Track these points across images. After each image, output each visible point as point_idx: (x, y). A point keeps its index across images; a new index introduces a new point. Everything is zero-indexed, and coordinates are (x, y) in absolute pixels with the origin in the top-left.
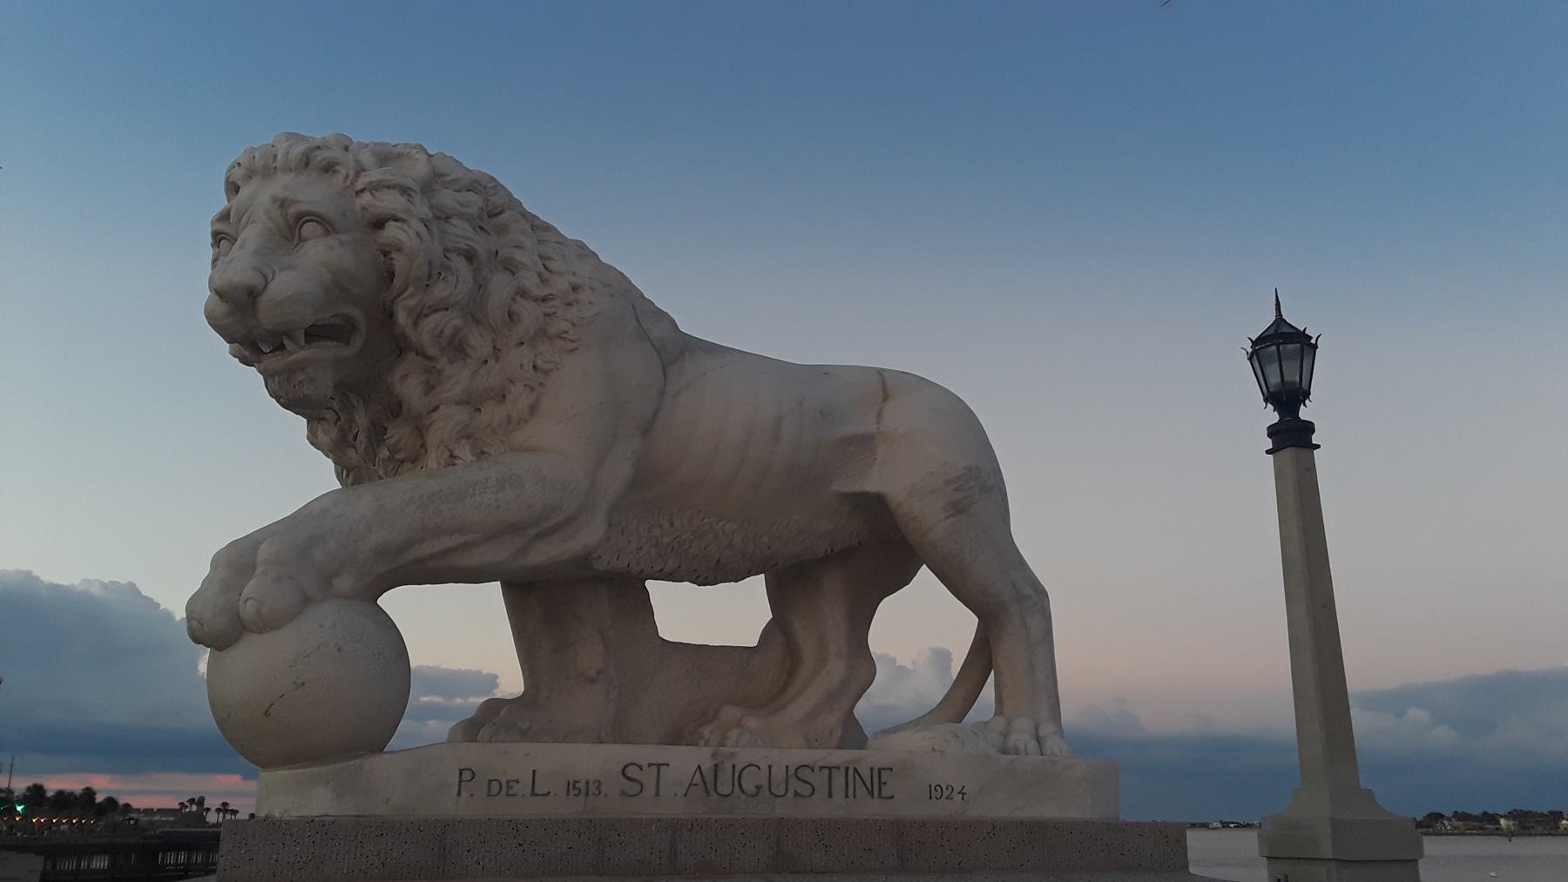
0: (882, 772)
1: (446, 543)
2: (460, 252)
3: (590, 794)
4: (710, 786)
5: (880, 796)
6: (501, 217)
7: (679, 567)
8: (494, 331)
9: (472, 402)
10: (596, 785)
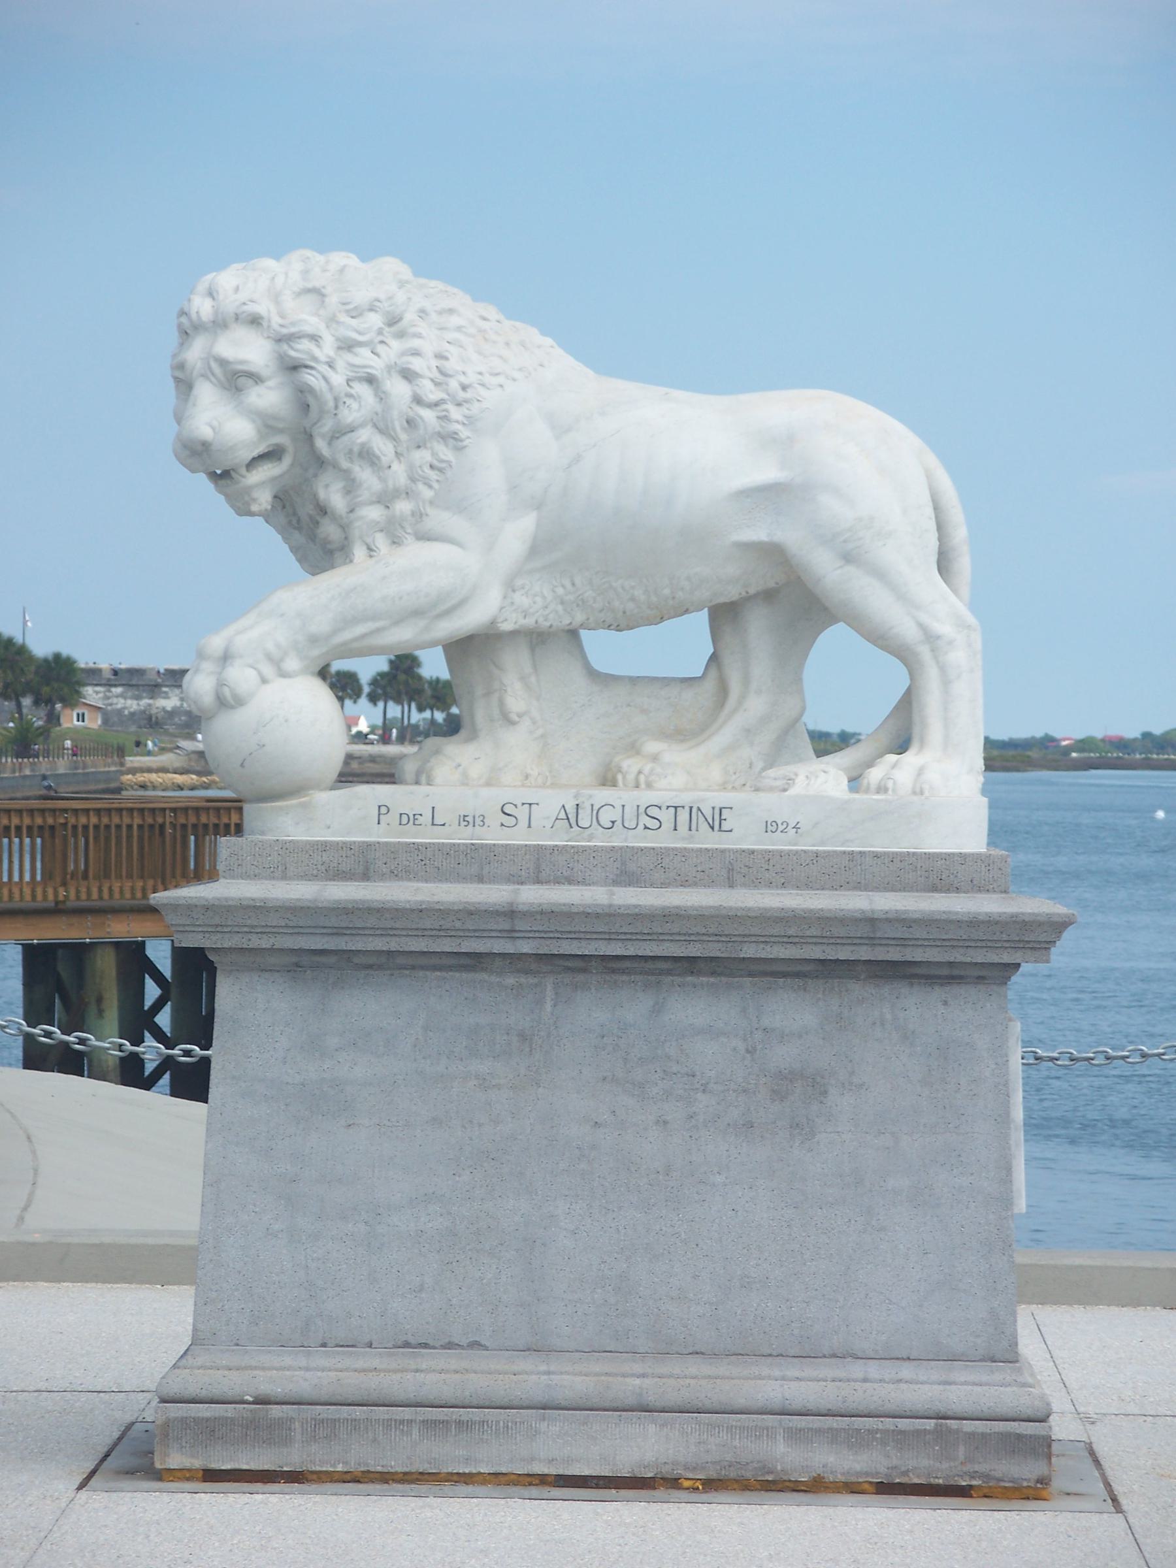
0: (723, 810)
1: (359, 630)
2: (360, 379)
3: (476, 824)
4: (573, 821)
5: (720, 830)
6: (399, 324)
7: (588, 619)
8: (395, 440)
9: (385, 499)
10: (481, 818)
